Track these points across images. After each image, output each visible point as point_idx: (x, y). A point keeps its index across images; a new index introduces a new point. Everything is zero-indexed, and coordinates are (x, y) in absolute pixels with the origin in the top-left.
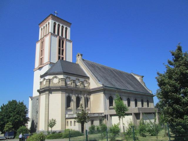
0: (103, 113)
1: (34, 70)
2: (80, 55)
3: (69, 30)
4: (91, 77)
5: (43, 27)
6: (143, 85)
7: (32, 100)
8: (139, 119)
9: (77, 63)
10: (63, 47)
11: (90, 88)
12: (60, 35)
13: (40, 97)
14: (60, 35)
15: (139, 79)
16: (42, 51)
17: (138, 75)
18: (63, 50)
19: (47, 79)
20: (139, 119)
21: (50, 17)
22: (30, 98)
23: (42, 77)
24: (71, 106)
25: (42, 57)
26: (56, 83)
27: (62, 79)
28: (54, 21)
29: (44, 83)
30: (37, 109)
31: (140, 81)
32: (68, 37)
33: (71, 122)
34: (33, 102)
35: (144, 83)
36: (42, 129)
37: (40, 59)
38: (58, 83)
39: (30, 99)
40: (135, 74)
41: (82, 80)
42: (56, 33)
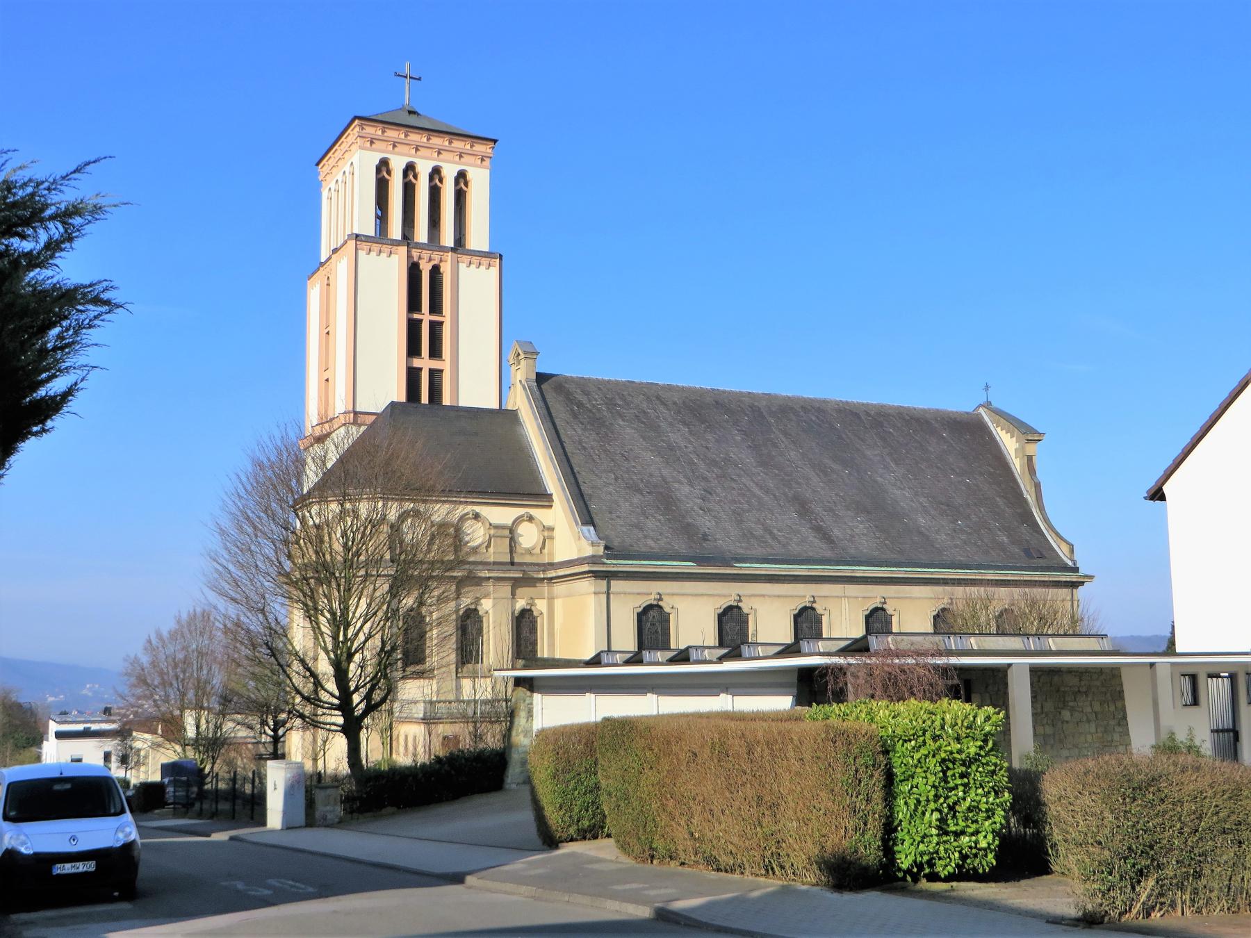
6: (1030, 498)
11: (551, 554)
21: (354, 131)
28: (375, 158)
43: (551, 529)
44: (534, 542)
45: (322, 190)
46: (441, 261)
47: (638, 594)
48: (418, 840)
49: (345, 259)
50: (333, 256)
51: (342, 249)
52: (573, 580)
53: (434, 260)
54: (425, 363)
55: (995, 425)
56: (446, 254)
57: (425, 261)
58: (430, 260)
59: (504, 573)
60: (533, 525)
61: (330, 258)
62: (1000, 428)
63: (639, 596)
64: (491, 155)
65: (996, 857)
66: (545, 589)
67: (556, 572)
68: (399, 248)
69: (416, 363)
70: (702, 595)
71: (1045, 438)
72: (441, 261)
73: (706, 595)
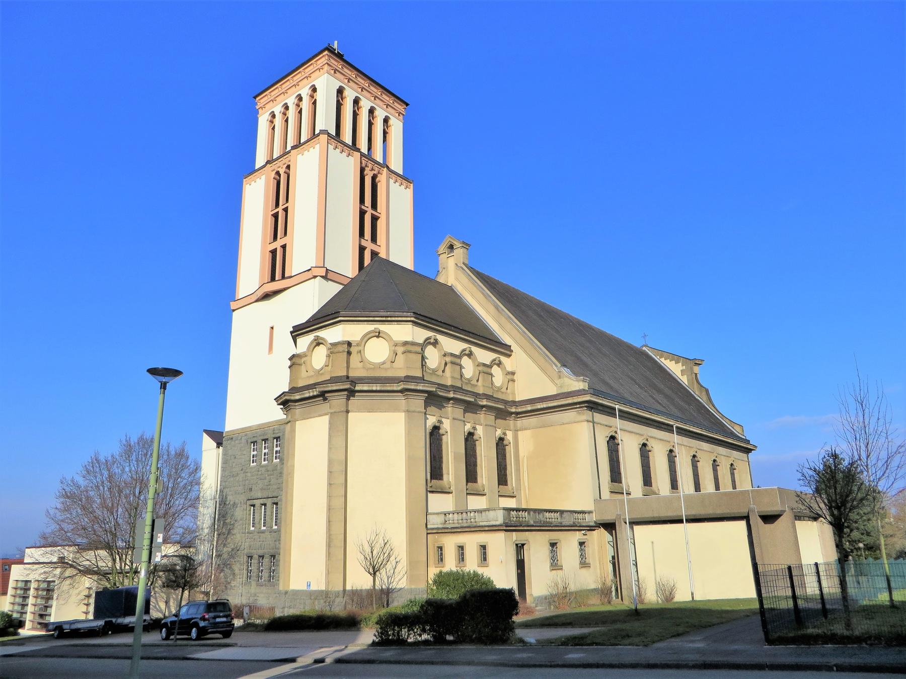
0: (590, 512)
1: (233, 305)
2: (457, 244)
3: (397, 127)
4: (516, 342)
5: (278, 109)
6: (703, 400)
7: (219, 444)
8: (134, 614)
9: (441, 279)
10: (374, 205)
11: (514, 394)
12: (363, 145)
13: (293, 431)
14: (363, 145)
15: (682, 371)
16: (276, 216)
17: (676, 358)
18: (375, 219)
19: (331, 340)
20: (134, 614)
21: (324, 58)
22: (206, 437)
23: (298, 331)
24: (445, 477)
25: (277, 245)
26: (382, 360)
27: (406, 343)
28: (337, 84)
29: (319, 358)
30: (251, 490)
31: (684, 380)
32: (396, 163)
33: (461, 548)
34: (224, 454)
35: (707, 391)
36: (309, 585)
37: (268, 256)
38: (388, 365)
39: (208, 443)
40: (662, 353)
41: (484, 356)
42: (347, 138)
43: (513, 373)
44: (501, 383)
45: (258, 116)
46: (379, 173)
47: (606, 426)
48: (652, 662)
49: (263, 177)
50: (292, 151)
51: (259, 172)
52: (552, 412)
53: (375, 171)
54: (367, 243)
55: (658, 357)
56: (382, 169)
57: (369, 169)
58: (372, 169)
59: (495, 404)
60: (499, 369)
61: (264, 166)
62: (664, 358)
63: (606, 427)
64: (404, 114)
65: (392, 639)
66: (511, 422)
67: (531, 406)
68: (354, 152)
69: (364, 243)
70: (632, 432)
71: (704, 363)
72: (379, 173)
73: (635, 433)
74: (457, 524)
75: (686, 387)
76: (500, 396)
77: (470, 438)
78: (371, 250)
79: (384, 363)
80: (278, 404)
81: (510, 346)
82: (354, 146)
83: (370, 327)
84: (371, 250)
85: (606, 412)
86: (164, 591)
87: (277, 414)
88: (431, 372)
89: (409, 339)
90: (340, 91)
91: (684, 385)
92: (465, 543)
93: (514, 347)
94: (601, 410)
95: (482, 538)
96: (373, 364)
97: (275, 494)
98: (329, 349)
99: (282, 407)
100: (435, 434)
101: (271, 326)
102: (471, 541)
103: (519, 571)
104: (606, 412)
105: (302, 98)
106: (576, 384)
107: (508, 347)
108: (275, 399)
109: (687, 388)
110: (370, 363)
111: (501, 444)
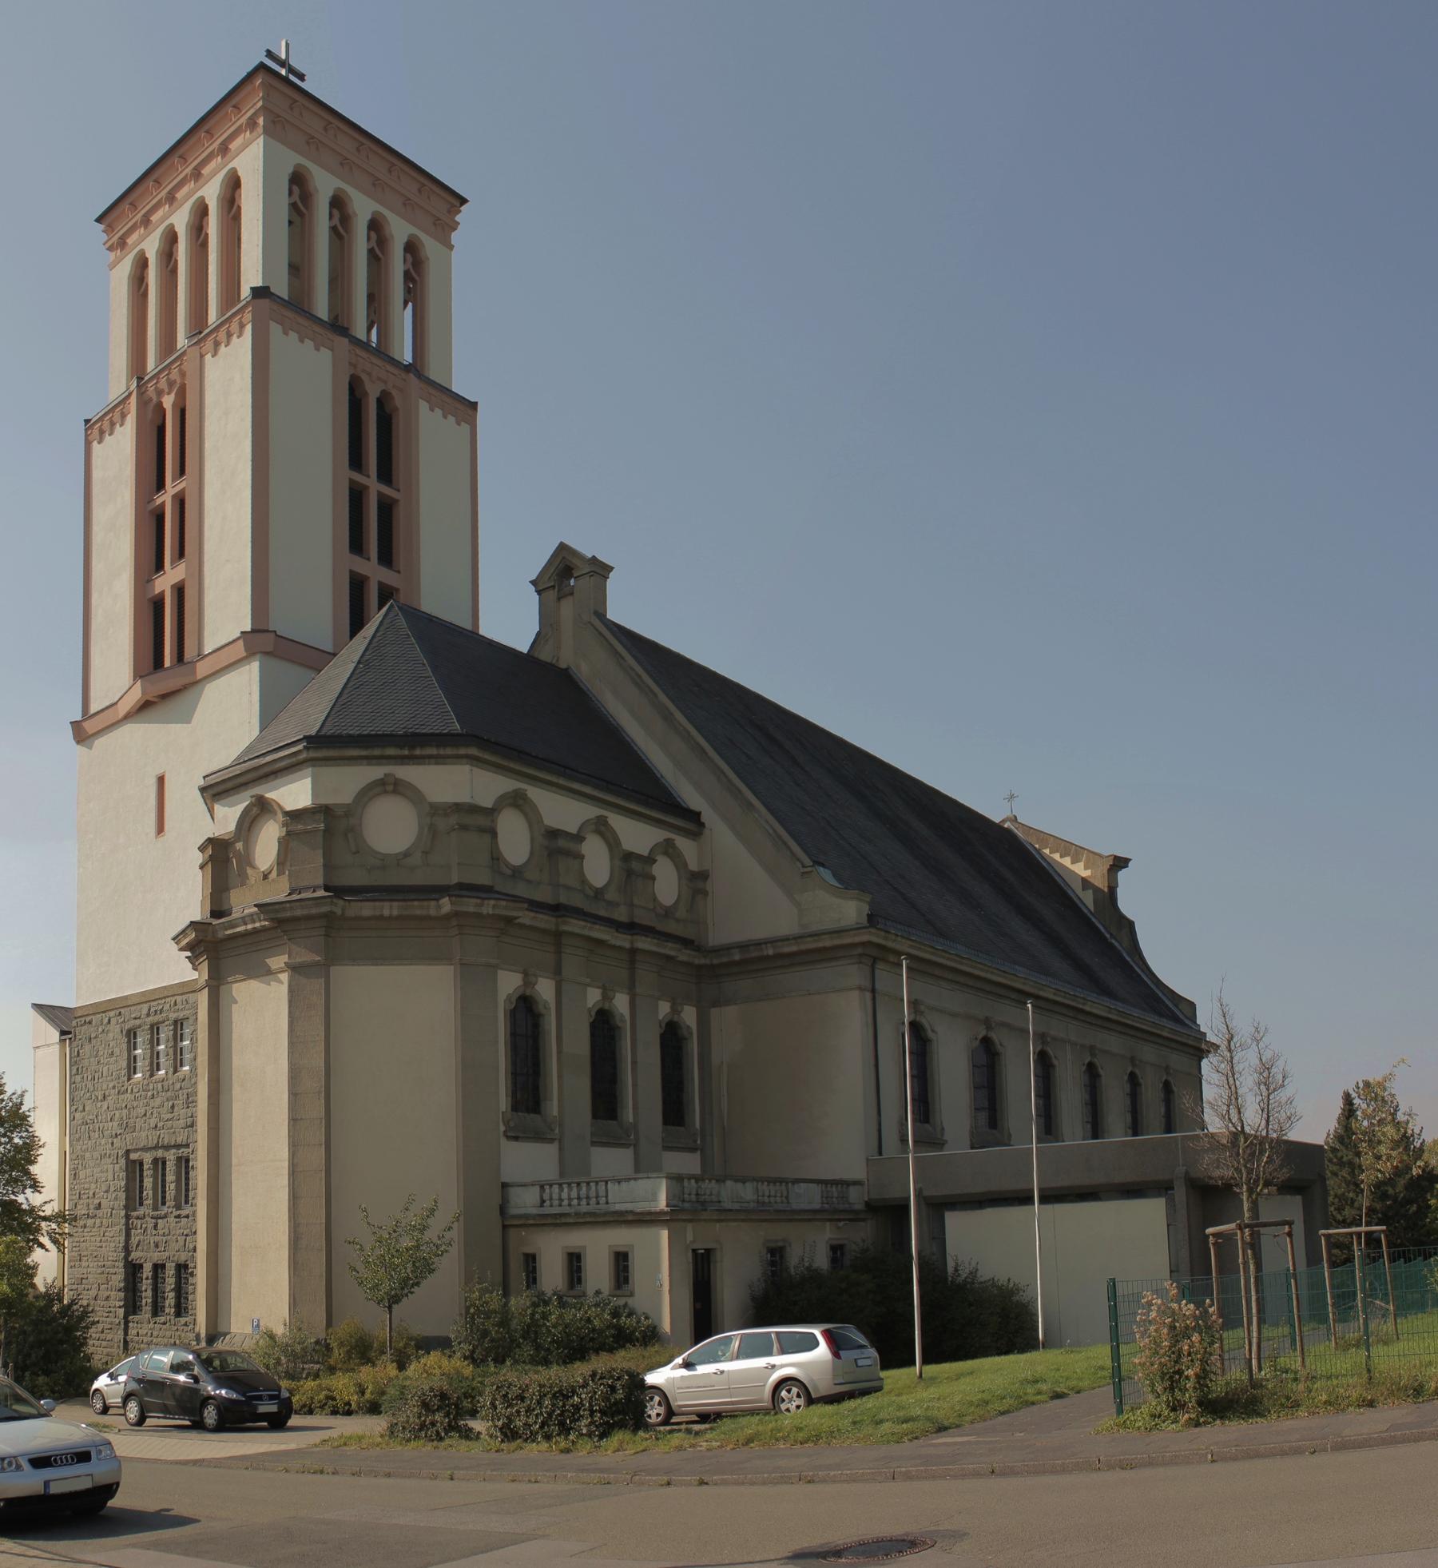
23: (216, 791)
27: (458, 807)
28: (291, 160)
74: (568, 1208)
75: (1089, 914)
76: (671, 927)
77: (603, 1026)
78: (351, 572)
79: (406, 854)
80: (181, 949)
81: (699, 814)
82: (338, 326)
83: (376, 772)
84: (351, 572)
85: (1105, 1027)
86: (519, 1096)
87: (179, 969)
88: (509, 872)
89: (463, 798)
90: (298, 180)
91: (1086, 911)
92: (585, 1247)
93: (708, 816)
94: (972, 987)
95: (620, 1237)
96: (384, 857)
97: (181, 1139)
98: (285, 824)
99: (189, 954)
100: (525, 1011)
101: (159, 772)
102: (597, 1246)
103: (699, 1306)
104: (1105, 1027)
105: (540, 585)
106: (849, 910)
107: (695, 817)
108: (174, 939)
109: (1091, 917)
110: (374, 854)
111: (672, 1038)
